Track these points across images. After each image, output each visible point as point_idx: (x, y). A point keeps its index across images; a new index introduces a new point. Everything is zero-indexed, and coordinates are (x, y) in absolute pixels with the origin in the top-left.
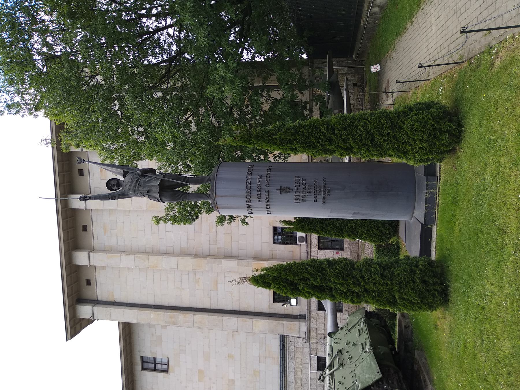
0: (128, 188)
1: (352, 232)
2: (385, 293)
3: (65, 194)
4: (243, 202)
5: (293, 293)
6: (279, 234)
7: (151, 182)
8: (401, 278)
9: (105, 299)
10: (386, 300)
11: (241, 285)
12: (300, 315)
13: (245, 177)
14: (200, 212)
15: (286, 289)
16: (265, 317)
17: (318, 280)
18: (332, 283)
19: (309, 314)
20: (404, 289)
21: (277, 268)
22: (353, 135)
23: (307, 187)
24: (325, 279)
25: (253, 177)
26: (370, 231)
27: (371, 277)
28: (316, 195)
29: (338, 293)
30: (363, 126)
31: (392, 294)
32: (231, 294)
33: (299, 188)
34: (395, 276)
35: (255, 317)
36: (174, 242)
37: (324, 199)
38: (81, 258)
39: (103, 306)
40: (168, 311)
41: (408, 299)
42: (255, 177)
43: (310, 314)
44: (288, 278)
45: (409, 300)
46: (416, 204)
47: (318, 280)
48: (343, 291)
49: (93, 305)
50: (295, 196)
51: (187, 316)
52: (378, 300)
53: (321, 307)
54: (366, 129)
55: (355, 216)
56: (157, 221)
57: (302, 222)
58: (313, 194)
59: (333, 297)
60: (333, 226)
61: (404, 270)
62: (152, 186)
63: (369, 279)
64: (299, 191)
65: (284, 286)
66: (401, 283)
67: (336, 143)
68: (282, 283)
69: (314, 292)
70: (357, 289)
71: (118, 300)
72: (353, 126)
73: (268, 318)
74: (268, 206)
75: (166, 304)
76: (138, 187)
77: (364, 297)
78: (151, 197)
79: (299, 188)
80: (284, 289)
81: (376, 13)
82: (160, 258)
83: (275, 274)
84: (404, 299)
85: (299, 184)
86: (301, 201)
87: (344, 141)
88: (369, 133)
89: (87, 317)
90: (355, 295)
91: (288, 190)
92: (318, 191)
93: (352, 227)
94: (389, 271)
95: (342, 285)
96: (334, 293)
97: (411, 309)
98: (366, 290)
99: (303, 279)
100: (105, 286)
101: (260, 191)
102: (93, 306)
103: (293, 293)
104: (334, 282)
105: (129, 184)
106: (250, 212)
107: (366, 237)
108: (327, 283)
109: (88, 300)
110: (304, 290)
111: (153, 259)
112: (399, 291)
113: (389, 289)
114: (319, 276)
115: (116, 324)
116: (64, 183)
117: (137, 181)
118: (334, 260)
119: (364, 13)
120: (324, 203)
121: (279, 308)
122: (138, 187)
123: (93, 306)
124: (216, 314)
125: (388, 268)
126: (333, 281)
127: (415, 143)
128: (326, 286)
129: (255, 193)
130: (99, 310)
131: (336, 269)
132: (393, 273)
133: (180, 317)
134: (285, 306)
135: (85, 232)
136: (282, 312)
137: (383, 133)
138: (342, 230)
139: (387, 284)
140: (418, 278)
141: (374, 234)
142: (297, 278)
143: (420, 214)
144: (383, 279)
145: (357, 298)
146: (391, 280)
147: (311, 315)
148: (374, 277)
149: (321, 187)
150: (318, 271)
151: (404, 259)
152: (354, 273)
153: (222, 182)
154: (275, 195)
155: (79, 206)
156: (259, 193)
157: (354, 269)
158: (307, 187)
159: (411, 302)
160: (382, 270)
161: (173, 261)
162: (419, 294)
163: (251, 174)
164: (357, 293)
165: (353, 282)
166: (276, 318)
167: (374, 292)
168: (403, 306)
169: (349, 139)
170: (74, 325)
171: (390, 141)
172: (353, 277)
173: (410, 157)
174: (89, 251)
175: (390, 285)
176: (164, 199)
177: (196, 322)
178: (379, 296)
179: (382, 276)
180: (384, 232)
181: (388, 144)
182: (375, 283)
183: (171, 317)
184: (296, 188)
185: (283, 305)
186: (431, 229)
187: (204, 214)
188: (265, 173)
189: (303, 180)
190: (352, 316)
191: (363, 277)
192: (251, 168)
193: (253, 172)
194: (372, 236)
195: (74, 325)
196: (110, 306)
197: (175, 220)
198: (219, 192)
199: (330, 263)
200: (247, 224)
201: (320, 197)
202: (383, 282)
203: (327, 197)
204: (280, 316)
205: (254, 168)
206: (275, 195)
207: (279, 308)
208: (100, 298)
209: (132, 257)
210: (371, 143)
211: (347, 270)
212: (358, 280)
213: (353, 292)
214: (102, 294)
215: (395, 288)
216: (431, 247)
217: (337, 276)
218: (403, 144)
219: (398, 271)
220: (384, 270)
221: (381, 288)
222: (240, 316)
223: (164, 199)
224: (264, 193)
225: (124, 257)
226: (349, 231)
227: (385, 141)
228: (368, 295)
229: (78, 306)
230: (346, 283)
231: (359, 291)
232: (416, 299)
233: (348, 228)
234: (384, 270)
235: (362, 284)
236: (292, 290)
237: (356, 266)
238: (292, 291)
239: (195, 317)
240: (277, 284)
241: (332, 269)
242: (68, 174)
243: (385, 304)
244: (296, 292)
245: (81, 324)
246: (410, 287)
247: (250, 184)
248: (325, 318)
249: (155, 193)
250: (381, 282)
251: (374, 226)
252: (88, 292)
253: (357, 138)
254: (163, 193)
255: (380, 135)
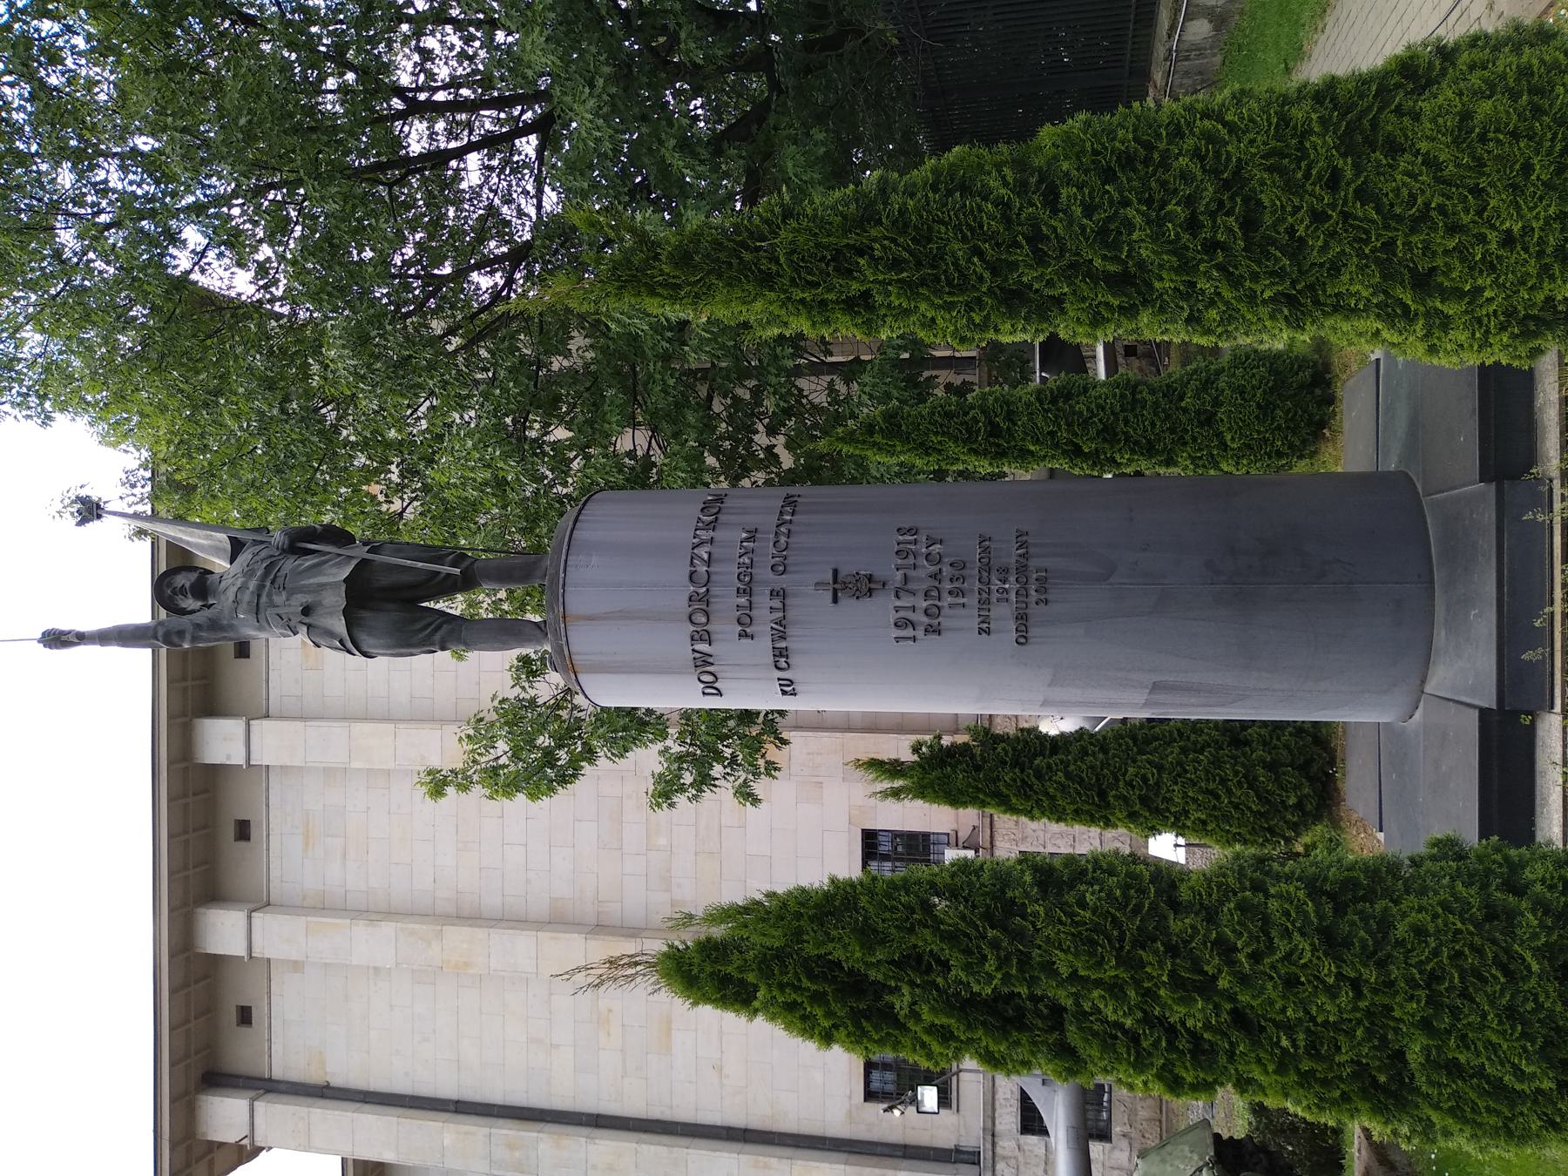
0: (231, 596)
1: (1144, 800)
2: (1350, 1034)
3: (184, 715)
4: (677, 641)
5: (864, 1034)
6: (885, 857)
7: (320, 574)
8: (1436, 953)
9: (295, 1075)
10: (1355, 1076)
11: (611, 997)
12: (958, 1150)
13: (686, 536)
14: (590, 755)
15: (829, 1014)
16: (835, 1155)
17: (990, 966)
18: (1062, 984)
19: (989, 1146)
20: (1455, 1013)
21: (784, 905)
22: (1149, 202)
23: (947, 571)
24: (1025, 961)
25: (718, 535)
26: (1218, 797)
27: (1271, 948)
28: (984, 603)
29: (1095, 1034)
30: (1197, 155)
31: (1383, 1039)
32: (719, 1069)
33: (911, 573)
34: (1400, 943)
35: (799, 1152)
36: (528, 881)
37: (1022, 619)
38: (224, 931)
39: (285, 1098)
40: (501, 1122)
41: (1480, 1072)
42: (730, 536)
43: (994, 1144)
44: (839, 954)
45: (1487, 1078)
46: (1440, 636)
47: (990, 966)
48: (1120, 1026)
49: (252, 1094)
50: (897, 609)
51: (565, 1142)
52: (1312, 1072)
53: (1032, 1122)
54: (1216, 172)
55: (1160, 697)
56: (438, 784)
57: (943, 764)
58: (972, 600)
59: (1068, 1060)
60: (1068, 775)
61: (1446, 907)
62: (322, 586)
63: (1255, 957)
64: (910, 586)
65: (817, 998)
66: (1433, 978)
67: (1062, 250)
68: (806, 983)
69: (969, 1027)
70: (1194, 1015)
71: (337, 1081)
72: (1147, 161)
73: (844, 1156)
74: (781, 656)
75: (497, 1097)
76: (269, 595)
77: (1231, 1055)
78: (319, 635)
79: (911, 573)
80: (819, 1012)
81: (1199, 49)
82: (480, 933)
83: (776, 939)
84: (1454, 1069)
85: (911, 560)
86: (920, 633)
87: (1106, 237)
88: (1234, 182)
89: (231, 1137)
90: (1183, 1044)
91: (866, 586)
92: (996, 584)
93: (1145, 779)
94: (1365, 918)
95: (1115, 990)
96: (1073, 1036)
97: (1495, 1133)
98: (1240, 1019)
99: (914, 962)
100: (295, 1035)
101: (747, 591)
102: (253, 1100)
103: (864, 1034)
104: (1074, 975)
105: (239, 584)
106: (709, 685)
107: (1204, 823)
108: (1032, 982)
109: (238, 1077)
110: (916, 1016)
111: (457, 936)
112: (1426, 1025)
113: (1369, 1013)
114: (995, 945)
115: (336, 1162)
116: (184, 679)
117: (268, 569)
118: (1070, 860)
119: (1160, 51)
120: (1023, 639)
121: (892, 1124)
122: (269, 595)
123: (253, 1100)
124: (665, 1139)
125: (1355, 900)
126: (1064, 971)
127: (1480, 213)
128: (1034, 999)
129: (727, 601)
130: (273, 1114)
131: (1082, 904)
132: (1386, 924)
133: (542, 1146)
134: (897, 1112)
135: (243, 844)
136: (895, 1137)
137: (1307, 176)
138: (1102, 794)
139: (1356, 985)
140: (1536, 952)
141: (1236, 807)
142: (880, 955)
143: (1466, 668)
144: (1338, 959)
145: (1197, 1064)
146: (1382, 964)
147: (999, 1150)
148: (1283, 946)
149: (1006, 570)
150: (988, 917)
151: (1433, 858)
152: (1175, 925)
153: (595, 560)
154: (811, 604)
155: (229, 757)
156: (743, 601)
157: (1176, 906)
158: (947, 571)
159: (1498, 1089)
160: (1328, 909)
161: (522, 948)
162: (1548, 1043)
163: (712, 526)
164: (1195, 1036)
165: (1173, 974)
166: (875, 1159)
167: (1289, 1028)
168: (1452, 1112)
169: (1130, 226)
170: (188, 1165)
171: (1346, 216)
172: (1172, 951)
173: (1451, 309)
174: (252, 906)
175: (1375, 991)
176: (367, 641)
177: (594, 1167)
178: (1313, 1050)
179: (1332, 943)
180: (1293, 772)
181: (1332, 234)
182: (1291, 983)
183: (511, 1147)
184: (899, 575)
185: (890, 1109)
186: (1531, 731)
187: (602, 762)
188: (774, 519)
189: (931, 542)
190: (1154, 1157)
191: (1226, 950)
192: (714, 509)
193: (722, 517)
194: (1227, 818)
195: (188, 1165)
196: (310, 1100)
197: (500, 782)
198: (576, 602)
199: (1052, 877)
200: (756, 801)
201: (1003, 614)
202: (1340, 976)
203: (1034, 610)
204: (886, 1151)
205: (728, 503)
206: (811, 604)
207: (892, 1124)
208: (277, 1073)
209: (388, 928)
210: (1246, 238)
211: (1137, 910)
212: (1197, 968)
213: (1171, 1031)
214: (286, 1061)
215: (1409, 1009)
216: (1533, 824)
217: (1086, 943)
218: (1413, 231)
219: (1414, 917)
220: (1340, 910)
221: (1328, 1009)
222: (749, 1147)
223: (367, 641)
224: (763, 601)
225: (361, 930)
226: (1134, 795)
227: (1318, 217)
228: (1255, 1044)
229: (203, 1097)
230: (1137, 984)
231: (1207, 1026)
232: (1529, 1070)
233: (1130, 784)
234: (1340, 910)
235: (1223, 983)
236: (856, 1016)
237: (1184, 894)
238: (858, 1025)
239: (591, 1147)
240: (782, 987)
241: (1062, 906)
242: (195, 647)
243: (1345, 1097)
244: (877, 1028)
245: (211, 1162)
246: (1492, 1003)
247: (709, 563)
248: (1048, 1162)
249: (331, 614)
250: (1328, 968)
251: (1236, 773)
252: (241, 1052)
253: (1170, 217)
254: (366, 614)
255: (1291, 187)
